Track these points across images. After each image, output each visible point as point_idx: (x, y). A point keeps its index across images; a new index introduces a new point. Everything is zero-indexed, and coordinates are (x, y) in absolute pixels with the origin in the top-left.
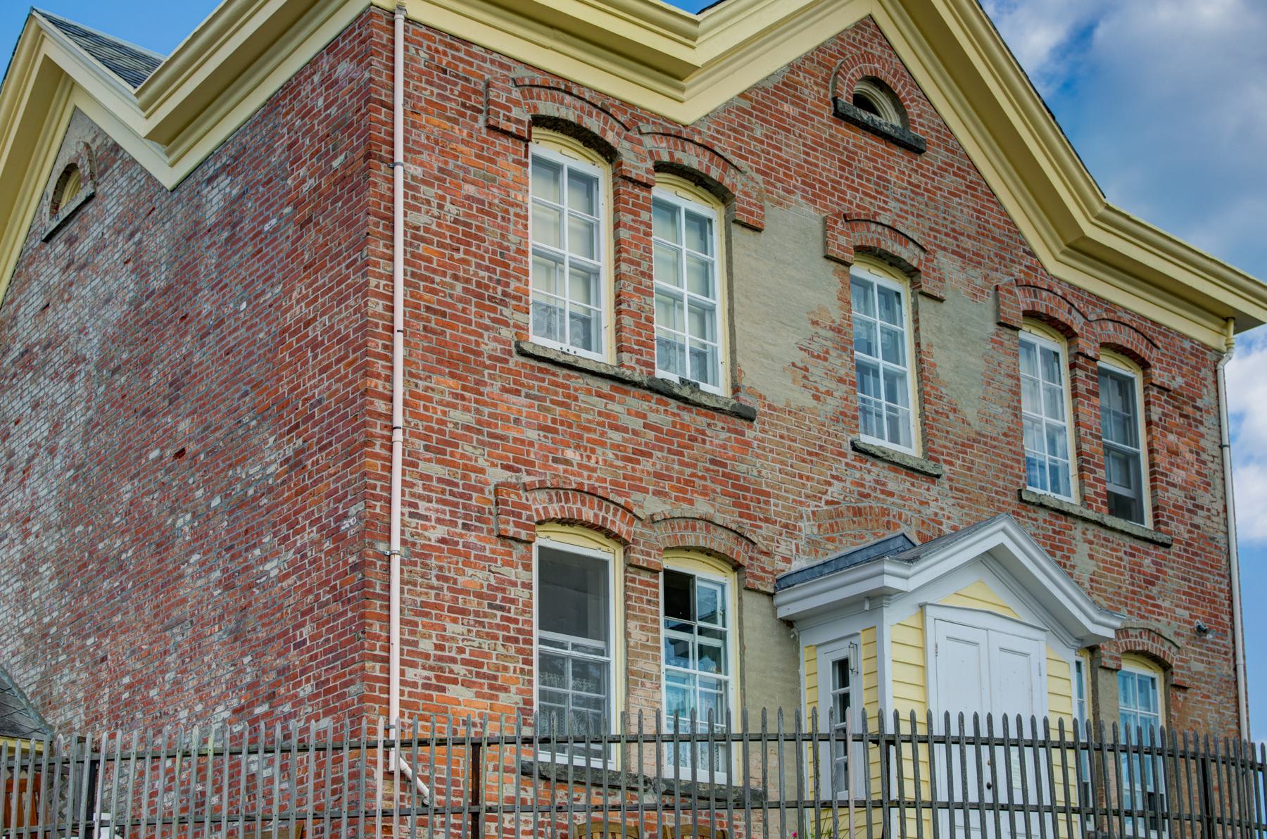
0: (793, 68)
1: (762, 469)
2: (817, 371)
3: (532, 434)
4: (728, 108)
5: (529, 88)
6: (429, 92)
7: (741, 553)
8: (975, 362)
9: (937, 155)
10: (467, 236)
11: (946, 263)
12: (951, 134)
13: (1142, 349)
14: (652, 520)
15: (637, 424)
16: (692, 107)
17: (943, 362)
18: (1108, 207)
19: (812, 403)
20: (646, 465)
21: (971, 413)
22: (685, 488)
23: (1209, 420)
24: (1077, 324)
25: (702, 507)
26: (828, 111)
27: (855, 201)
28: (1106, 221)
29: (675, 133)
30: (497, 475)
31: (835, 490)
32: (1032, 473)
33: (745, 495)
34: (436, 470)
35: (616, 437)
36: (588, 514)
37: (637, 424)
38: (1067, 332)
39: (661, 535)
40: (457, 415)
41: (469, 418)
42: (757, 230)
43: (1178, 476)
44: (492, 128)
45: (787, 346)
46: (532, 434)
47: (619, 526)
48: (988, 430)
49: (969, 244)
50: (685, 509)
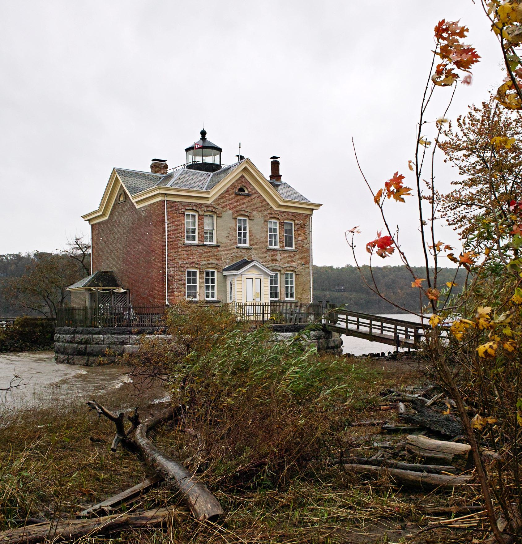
0: (228, 188)
1: (221, 253)
2: (231, 237)
3: (186, 256)
4: (216, 199)
5: (184, 206)
6: (170, 210)
7: (217, 267)
8: (259, 228)
9: (254, 195)
10: (176, 229)
11: (255, 213)
12: (257, 191)
13: (294, 218)
14: (203, 265)
15: (201, 251)
16: (209, 202)
17: (253, 230)
18: (280, 206)
19: (229, 241)
20: (202, 256)
21: (258, 237)
22: (209, 259)
23: (308, 227)
24: (280, 217)
25: (211, 261)
26: (234, 194)
27: (238, 208)
28: (284, 201)
29: (207, 206)
30: (180, 262)
31: (233, 254)
32: (110, 438)
33: (218, 258)
34: (172, 263)
35: (198, 253)
36: (193, 266)
37: (201, 251)
38: (278, 219)
39: (205, 267)
40: (175, 255)
41: (176, 255)
42: (221, 217)
43: (300, 238)
44: (180, 213)
45: (226, 234)
46: (186, 256)
47: (198, 266)
48: (261, 239)
49: (259, 209)
50: (209, 262)
